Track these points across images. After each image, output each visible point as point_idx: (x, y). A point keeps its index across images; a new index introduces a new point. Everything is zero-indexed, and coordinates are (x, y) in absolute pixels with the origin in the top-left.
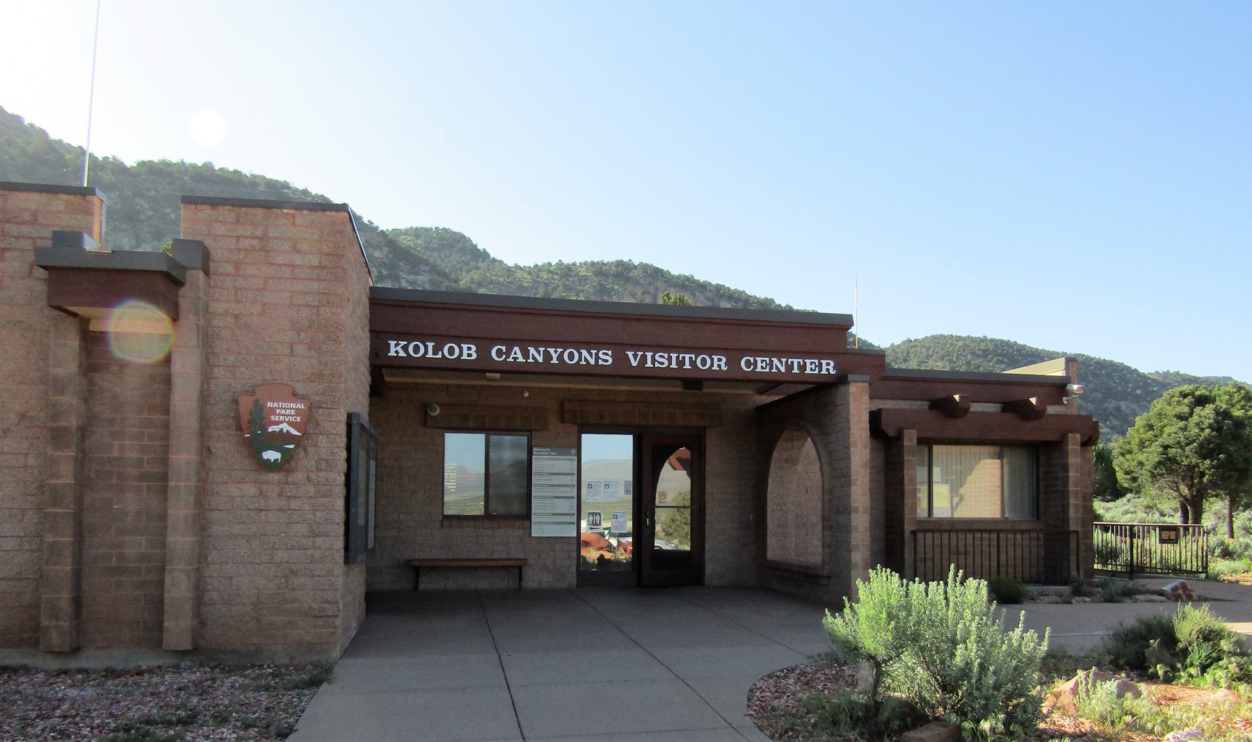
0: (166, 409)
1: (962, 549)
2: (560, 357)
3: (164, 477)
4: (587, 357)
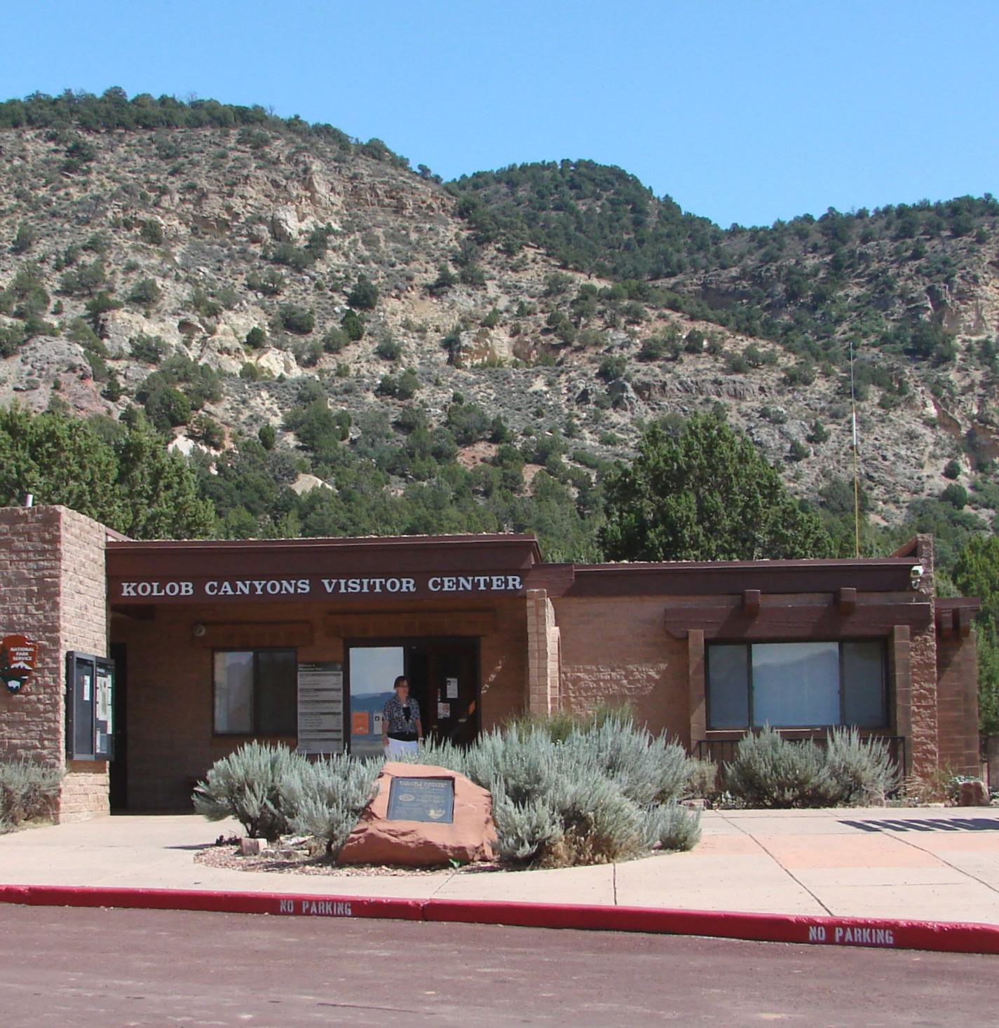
4: (288, 587)
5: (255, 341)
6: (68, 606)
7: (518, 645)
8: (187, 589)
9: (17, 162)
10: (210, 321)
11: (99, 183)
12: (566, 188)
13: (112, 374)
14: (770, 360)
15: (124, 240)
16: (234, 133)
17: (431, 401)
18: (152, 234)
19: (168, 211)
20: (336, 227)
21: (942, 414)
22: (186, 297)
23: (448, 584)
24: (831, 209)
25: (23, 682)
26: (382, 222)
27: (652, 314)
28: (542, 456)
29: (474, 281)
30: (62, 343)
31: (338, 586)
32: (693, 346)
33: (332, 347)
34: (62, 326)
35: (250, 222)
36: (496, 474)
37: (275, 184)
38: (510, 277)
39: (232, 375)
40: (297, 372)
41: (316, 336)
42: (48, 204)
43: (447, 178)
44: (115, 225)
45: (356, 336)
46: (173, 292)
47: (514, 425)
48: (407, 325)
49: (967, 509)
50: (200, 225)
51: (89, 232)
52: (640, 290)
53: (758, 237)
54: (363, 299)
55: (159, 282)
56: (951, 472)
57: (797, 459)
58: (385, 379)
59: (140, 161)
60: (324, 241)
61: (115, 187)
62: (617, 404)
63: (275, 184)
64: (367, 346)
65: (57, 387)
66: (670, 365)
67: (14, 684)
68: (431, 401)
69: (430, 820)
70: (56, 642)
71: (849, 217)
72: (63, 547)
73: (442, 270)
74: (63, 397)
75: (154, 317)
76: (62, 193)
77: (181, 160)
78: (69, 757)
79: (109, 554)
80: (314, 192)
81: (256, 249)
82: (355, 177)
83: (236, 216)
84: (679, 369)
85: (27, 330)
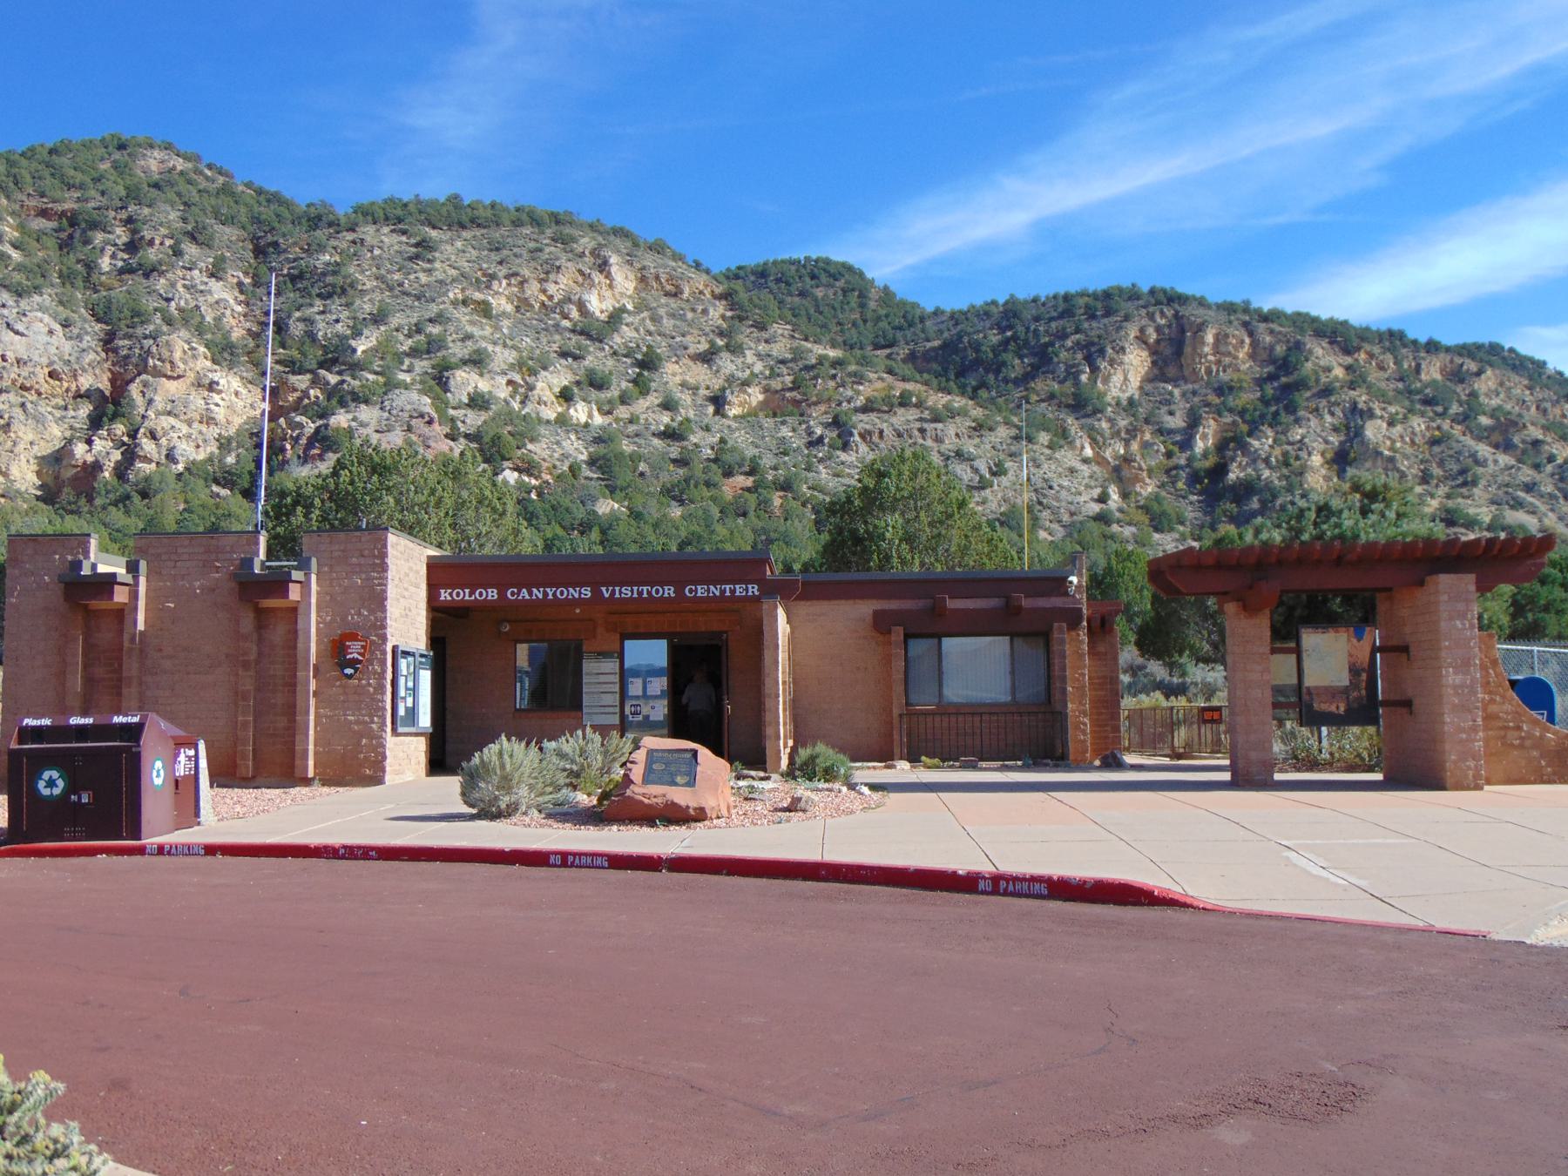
0: (295, 647)
1: (969, 731)
2: (554, 594)
3: (295, 685)
4: (574, 593)
5: (566, 396)
6: (393, 609)
7: (757, 638)
8: (492, 594)
9: (377, 252)
10: (530, 380)
11: (441, 270)
12: (807, 279)
13: (453, 420)
14: (962, 412)
15: (463, 316)
16: (549, 232)
17: (703, 443)
18: (484, 310)
19: (497, 293)
20: (630, 307)
21: (1097, 454)
22: (511, 360)
23: (701, 591)
24: (1012, 296)
25: (356, 670)
26: (664, 305)
27: (872, 376)
28: (786, 486)
29: (735, 349)
30: (414, 396)
31: (613, 592)
32: (904, 401)
33: (624, 399)
34: (414, 381)
35: (561, 303)
36: (752, 499)
37: (580, 271)
38: (762, 347)
39: (548, 422)
40: (598, 420)
41: (614, 393)
42: (401, 285)
43: (715, 270)
44: (455, 303)
45: (645, 392)
46: (502, 357)
47: (767, 461)
48: (684, 385)
49: (1115, 528)
50: (522, 304)
51: (434, 309)
52: (864, 357)
53: (956, 318)
54: (648, 363)
55: (490, 348)
56: (1103, 499)
57: (983, 488)
58: (667, 426)
59: (474, 253)
60: (621, 318)
61: (454, 272)
62: (845, 447)
63: (580, 271)
64: (653, 399)
65: (409, 429)
66: (886, 416)
67: (349, 671)
68: (703, 443)
69: (676, 784)
70: (384, 639)
71: (1026, 302)
72: (389, 561)
73: (712, 343)
74: (414, 438)
75: (487, 376)
76: (412, 277)
77: (505, 252)
78: (394, 730)
79: (429, 567)
80: (612, 280)
81: (566, 323)
82: (644, 268)
83: (551, 298)
84: (894, 420)
85: (385, 384)
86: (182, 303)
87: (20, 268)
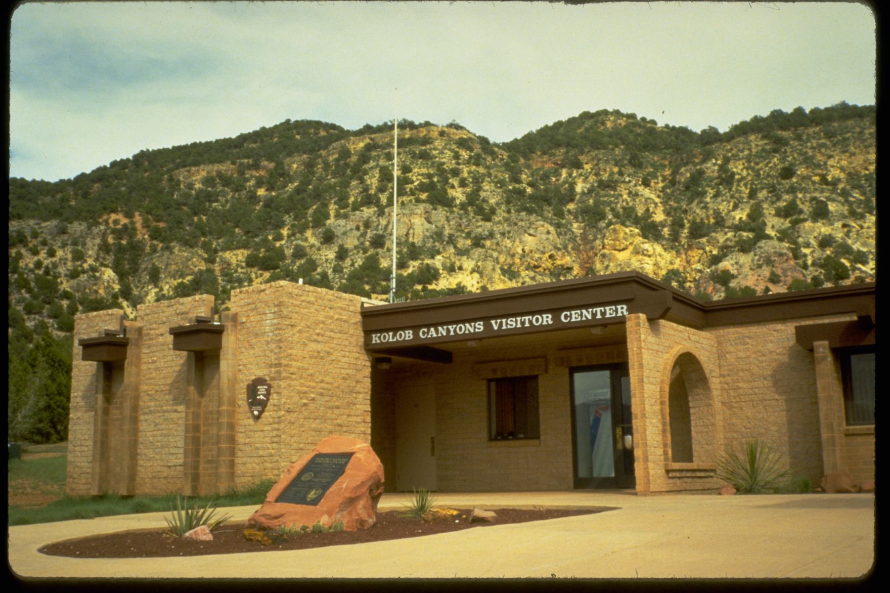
86: (624, 204)
87: (531, 197)
